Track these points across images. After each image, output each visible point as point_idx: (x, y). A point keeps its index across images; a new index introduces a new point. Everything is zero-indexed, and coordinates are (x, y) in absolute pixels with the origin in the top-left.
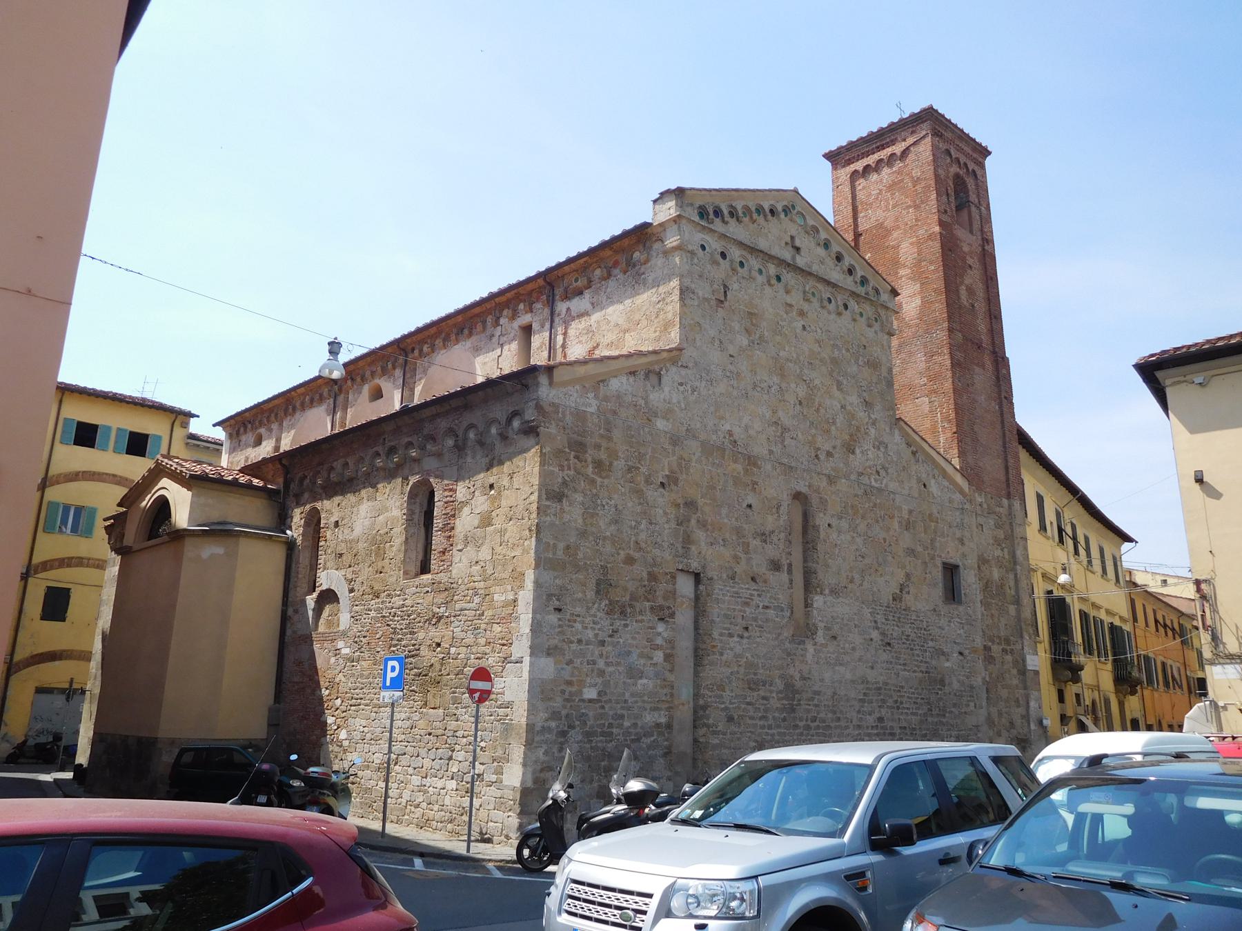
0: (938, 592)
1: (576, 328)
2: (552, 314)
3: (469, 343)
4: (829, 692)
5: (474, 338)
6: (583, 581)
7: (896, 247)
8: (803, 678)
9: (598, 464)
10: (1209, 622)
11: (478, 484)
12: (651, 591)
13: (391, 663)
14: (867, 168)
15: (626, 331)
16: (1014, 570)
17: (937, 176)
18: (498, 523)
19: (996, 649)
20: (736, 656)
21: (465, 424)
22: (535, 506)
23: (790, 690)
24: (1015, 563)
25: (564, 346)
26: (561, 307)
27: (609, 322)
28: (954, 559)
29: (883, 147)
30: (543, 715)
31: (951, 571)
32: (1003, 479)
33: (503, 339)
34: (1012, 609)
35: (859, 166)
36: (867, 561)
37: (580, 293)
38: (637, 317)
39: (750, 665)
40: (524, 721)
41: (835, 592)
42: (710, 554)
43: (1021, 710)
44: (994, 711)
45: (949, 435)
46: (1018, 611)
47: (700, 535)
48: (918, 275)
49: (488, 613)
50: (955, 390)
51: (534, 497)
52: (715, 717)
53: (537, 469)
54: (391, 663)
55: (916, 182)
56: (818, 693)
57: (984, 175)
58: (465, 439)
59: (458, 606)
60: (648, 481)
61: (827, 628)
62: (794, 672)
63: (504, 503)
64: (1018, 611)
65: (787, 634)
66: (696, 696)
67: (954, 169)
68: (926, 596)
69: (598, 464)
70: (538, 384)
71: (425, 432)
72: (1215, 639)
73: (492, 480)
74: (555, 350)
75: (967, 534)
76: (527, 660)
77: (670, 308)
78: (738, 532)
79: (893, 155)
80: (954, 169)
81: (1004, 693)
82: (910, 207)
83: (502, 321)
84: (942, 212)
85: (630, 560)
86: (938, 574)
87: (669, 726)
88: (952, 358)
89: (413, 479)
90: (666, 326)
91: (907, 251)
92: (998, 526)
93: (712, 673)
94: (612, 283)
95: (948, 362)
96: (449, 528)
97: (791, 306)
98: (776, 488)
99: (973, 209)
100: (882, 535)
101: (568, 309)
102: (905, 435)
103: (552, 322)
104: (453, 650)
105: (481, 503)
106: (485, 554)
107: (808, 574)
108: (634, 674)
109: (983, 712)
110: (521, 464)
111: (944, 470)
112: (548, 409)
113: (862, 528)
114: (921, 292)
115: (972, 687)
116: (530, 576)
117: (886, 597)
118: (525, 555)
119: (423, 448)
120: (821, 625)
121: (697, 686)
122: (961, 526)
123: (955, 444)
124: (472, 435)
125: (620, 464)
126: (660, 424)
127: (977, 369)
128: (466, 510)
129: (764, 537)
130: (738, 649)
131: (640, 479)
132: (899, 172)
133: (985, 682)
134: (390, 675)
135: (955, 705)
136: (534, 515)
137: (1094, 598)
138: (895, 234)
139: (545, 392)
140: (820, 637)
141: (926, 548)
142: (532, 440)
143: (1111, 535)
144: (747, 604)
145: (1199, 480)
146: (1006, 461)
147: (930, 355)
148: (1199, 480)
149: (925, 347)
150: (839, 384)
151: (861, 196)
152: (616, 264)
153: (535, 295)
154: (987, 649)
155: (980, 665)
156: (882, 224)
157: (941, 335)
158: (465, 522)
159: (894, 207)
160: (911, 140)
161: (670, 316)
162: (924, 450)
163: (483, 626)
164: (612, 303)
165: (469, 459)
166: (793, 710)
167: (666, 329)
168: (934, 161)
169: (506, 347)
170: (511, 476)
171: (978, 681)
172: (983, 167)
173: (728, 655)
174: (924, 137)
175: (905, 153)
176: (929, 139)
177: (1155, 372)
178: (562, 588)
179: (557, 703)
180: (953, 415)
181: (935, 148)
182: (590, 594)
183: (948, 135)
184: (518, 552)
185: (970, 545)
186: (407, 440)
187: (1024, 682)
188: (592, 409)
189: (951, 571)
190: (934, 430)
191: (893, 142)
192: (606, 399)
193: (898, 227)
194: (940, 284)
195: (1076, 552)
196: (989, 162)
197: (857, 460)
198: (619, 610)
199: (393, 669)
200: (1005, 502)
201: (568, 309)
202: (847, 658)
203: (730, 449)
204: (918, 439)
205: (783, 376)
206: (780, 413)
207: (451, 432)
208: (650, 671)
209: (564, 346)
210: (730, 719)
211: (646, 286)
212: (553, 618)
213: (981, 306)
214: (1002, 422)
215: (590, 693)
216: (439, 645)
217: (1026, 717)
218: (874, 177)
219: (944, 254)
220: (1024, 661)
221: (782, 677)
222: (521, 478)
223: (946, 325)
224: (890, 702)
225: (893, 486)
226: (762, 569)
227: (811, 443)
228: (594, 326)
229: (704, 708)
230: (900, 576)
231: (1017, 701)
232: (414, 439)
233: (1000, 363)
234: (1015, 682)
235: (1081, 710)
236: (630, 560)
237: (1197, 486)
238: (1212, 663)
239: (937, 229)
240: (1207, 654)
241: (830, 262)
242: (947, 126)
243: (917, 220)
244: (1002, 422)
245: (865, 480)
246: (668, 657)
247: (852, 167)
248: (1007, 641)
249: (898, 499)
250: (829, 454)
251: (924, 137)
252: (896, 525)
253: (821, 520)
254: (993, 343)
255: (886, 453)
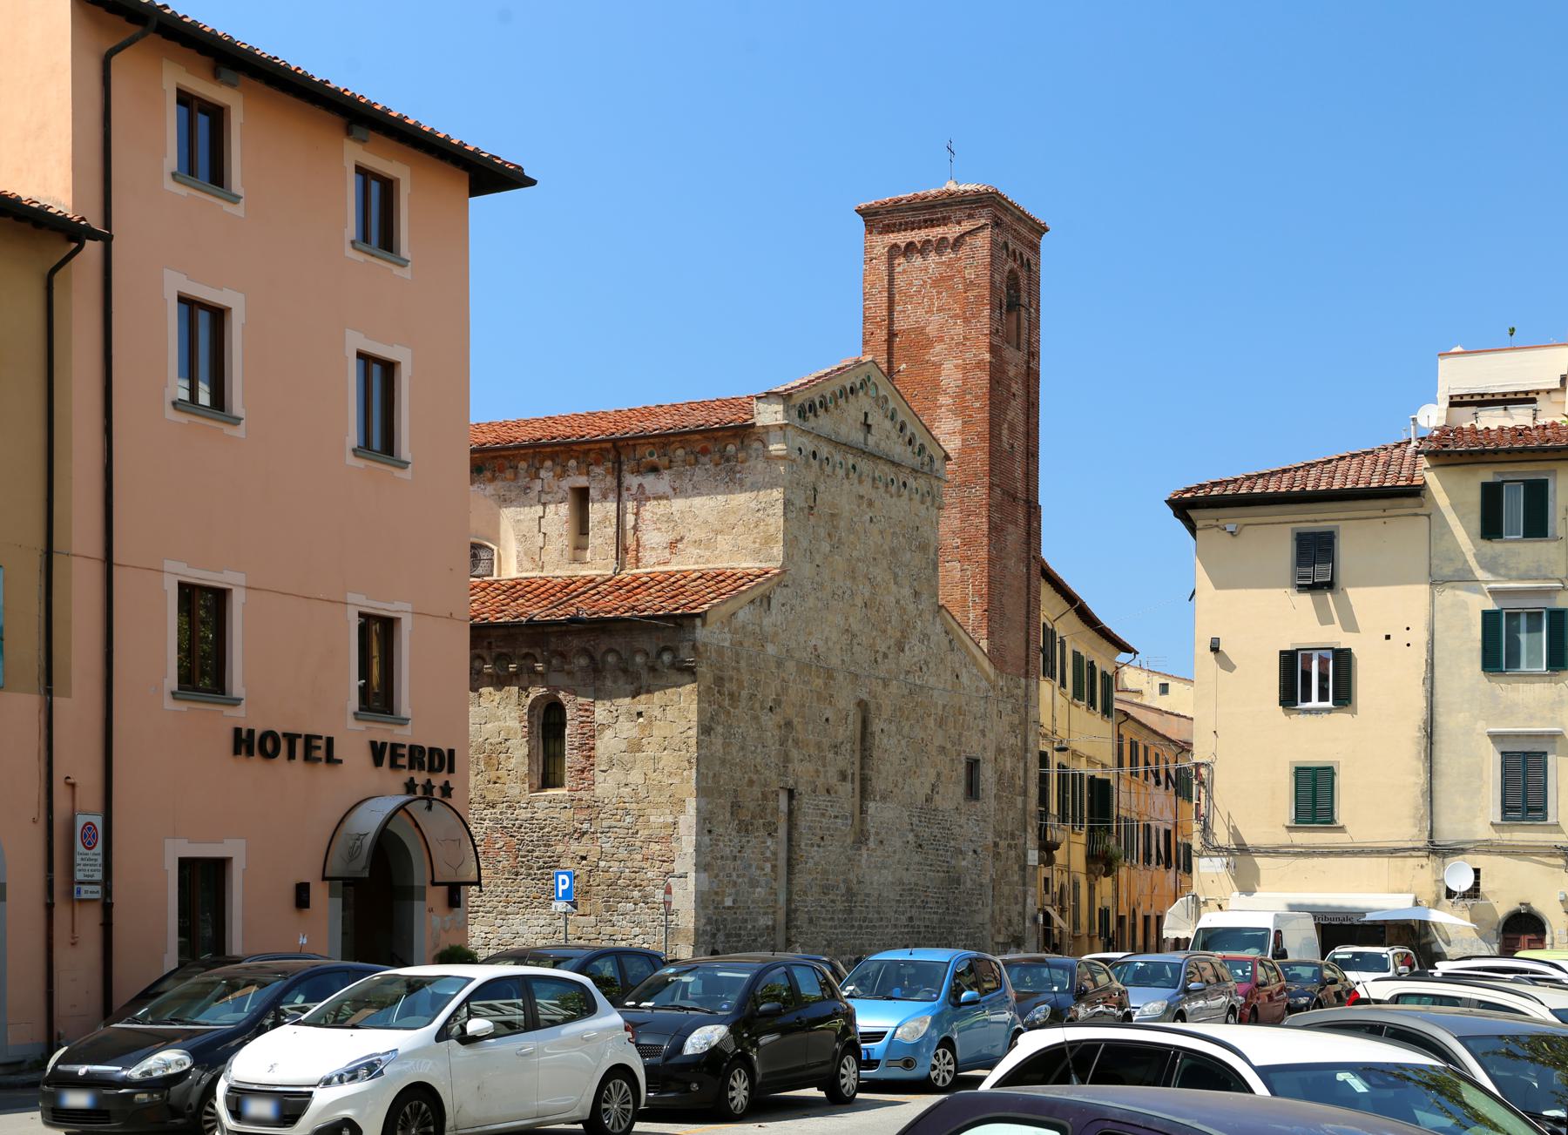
0: (961, 789)
1: (651, 509)
2: (619, 485)
3: (490, 489)
4: (876, 894)
5: (499, 484)
6: (738, 806)
7: (938, 366)
8: (859, 882)
9: (731, 695)
10: (1203, 811)
11: (622, 710)
12: (764, 809)
13: (561, 877)
14: (910, 245)
15: (717, 532)
16: (1025, 758)
17: (992, 283)
18: (650, 751)
19: (1003, 844)
20: (816, 864)
21: (603, 648)
22: (694, 741)
23: (850, 894)
24: (1026, 750)
25: (635, 528)
26: (632, 481)
27: (696, 516)
28: (976, 752)
29: (930, 223)
30: (703, 921)
31: (973, 765)
32: (1023, 655)
33: (544, 498)
34: (1019, 799)
35: (901, 238)
36: (909, 763)
37: (654, 469)
38: (732, 520)
39: (825, 872)
40: (691, 926)
41: (884, 798)
42: (802, 771)
43: (1019, 908)
44: (997, 907)
45: (979, 612)
46: (1025, 803)
47: (794, 753)
48: (960, 410)
49: (643, 833)
50: (990, 560)
51: (693, 732)
52: (801, 920)
53: (694, 706)
54: (561, 877)
55: (969, 285)
56: (868, 895)
57: (1038, 264)
58: (604, 662)
59: (605, 824)
60: (762, 708)
61: (877, 834)
62: (852, 876)
63: (655, 732)
64: (1025, 803)
65: (849, 840)
66: (789, 901)
67: (1010, 264)
68: (954, 791)
69: (731, 695)
70: (694, 627)
71: (552, 647)
72: (1206, 830)
73: (640, 708)
74: (624, 530)
75: (988, 724)
76: (692, 875)
77: (771, 520)
78: (819, 745)
79: (944, 239)
80: (1010, 264)
81: (1006, 890)
82: (956, 316)
83: (543, 473)
84: (994, 333)
85: (751, 783)
86: (962, 769)
87: (774, 928)
88: (990, 522)
89: (536, 692)
90: (768, 540)
91: (950, 375)
92: (1014, 711)
93: (801, 880)
94: (699, 472)
95: (985, 527)
96: (588, 749)
97: (862, 497)
98: (845, 700)
99: (1023, 313)
100: (922, 734)
101: (640, 485)
102: (944, 623)
103: (620, 495)
104: (602, 864)
105: (627, 729)
106: (636, 777)
107: (864, 781)
108: (754, 883)
109: (988, 910)
110: (675, 698)
111: (974, 657)
112: (701, 649)
113: (906, 729)
114: (962, 432)
115: (981, 885)
116: (691, 805)
117: (921, 798)
118: (687, 783)
119: (547, 663)
120: (873, 831)
121: (789, 892)
122: (984, 717)
123: (985, 624)
124: (611, 659)
125: (744, 693)
126: (771, 649)
127: (1011, 528)
128: (609, 733)
129: (835, 748)
130: (817, 858)
131: (757, 705)
132: (949, 265)
133: (993, 880)
134: (561, 887)
135: (967, 904)
136: (694, 749)
137: (1076, 744)
138: (938, 348)
139: (701, 634)
140: (872, 845)
141: (954, 744)
142: (687, 678)
143: (1105, 644)
144: (823, 815)
145: (1215, 649)
146: (1028, 633)
147: (967, 514)
148: (1215, 649)
149: (962, 502)
150: (896, 576)
151: (900, 281)
152: (705, 451)
153: (592, 455)
154: (996, 845)
155: (989, 862)
156: (924, 328)
157: (980, 492)
158: (607, 744)
159: (939, 310)
160: (967, 226)
161: (772, 530)
162: (963, 642)
163: (638, 844)
164: (700, 494)
165: (609, 683)
166: (851, 912)
167: (767, 543)
168: (992, 264)
169: (551, 508)
170: (664, 708)
171: (986, 879)
172: (1035, 248)
173: (810, 864)
174: (982, 228)
175: (958, 242)
176: (987, 232)
177: (1185, 508)
178: (712, 812)
179: (710, 911)
180: (985, 591)
181: (993, 243)
182: (728, 815)
183: (1007, 219)
184: (676, 780)
185: (987, 737)
186: (525, 650)
187: (1024, 877)
188: (727, 644)
189: (973, 765)
190: (964, 607)
191: (944, 221)
192: (735, 632)
193: (941, 339)
194: (983, 428)
195: (1063, 684)
196: (1045, 242)
197: (906, 659)
198: (744, 828)
199: (564, 882)
200: (1023, 681)
201: (640, 485)
202: (890, 861)
203: (817, 666)
204: (955, 626)
205: (854, 578)
206: (851, 620)
207: (585, 652)
208: (763, 880)
209: (635, 528)
210: (811, 921)
211: (742, 488)
212: (707, 839)
213: (1019, 445)
214: (1028, 587)
215: (728, 902)
216: (583, 858)
217: (1022, 915)
218: (917, 261)
219: (992, 389)
220: (1025, 855)
221: (845, 881)
222: (676, 711)
223: (986, 479)
224: (918, 902)
225: (932, 681)
226: (834, 780)
227: (872, 646)
228: (677, 516)
229: (796, 910)
230: (933, 772)
231: (1016, 897)
232: (537, 652)
233: (1033, 511)
234: (1016, 878)
235: (1048, 899)
236: (751, 783)
237: (1212, 655)
238: (1200, 856)
239: (987, 356)
240: (1196, 846)
241: (894, 434)
242: (1007, 209)
243: (965, 338)
244: (1028, 587)
245: (910, 679)
246: (774, 867)
247: (893, 238)
248: (1013, 836)
249: (936, 693)
250: (885, 656)
251: (982, 228)
252: (932, 723)
253: (877, 725)
254: (1028, 490)
255: (928, 647)
